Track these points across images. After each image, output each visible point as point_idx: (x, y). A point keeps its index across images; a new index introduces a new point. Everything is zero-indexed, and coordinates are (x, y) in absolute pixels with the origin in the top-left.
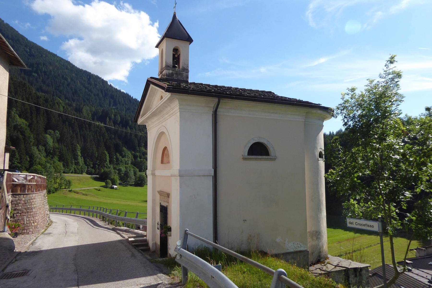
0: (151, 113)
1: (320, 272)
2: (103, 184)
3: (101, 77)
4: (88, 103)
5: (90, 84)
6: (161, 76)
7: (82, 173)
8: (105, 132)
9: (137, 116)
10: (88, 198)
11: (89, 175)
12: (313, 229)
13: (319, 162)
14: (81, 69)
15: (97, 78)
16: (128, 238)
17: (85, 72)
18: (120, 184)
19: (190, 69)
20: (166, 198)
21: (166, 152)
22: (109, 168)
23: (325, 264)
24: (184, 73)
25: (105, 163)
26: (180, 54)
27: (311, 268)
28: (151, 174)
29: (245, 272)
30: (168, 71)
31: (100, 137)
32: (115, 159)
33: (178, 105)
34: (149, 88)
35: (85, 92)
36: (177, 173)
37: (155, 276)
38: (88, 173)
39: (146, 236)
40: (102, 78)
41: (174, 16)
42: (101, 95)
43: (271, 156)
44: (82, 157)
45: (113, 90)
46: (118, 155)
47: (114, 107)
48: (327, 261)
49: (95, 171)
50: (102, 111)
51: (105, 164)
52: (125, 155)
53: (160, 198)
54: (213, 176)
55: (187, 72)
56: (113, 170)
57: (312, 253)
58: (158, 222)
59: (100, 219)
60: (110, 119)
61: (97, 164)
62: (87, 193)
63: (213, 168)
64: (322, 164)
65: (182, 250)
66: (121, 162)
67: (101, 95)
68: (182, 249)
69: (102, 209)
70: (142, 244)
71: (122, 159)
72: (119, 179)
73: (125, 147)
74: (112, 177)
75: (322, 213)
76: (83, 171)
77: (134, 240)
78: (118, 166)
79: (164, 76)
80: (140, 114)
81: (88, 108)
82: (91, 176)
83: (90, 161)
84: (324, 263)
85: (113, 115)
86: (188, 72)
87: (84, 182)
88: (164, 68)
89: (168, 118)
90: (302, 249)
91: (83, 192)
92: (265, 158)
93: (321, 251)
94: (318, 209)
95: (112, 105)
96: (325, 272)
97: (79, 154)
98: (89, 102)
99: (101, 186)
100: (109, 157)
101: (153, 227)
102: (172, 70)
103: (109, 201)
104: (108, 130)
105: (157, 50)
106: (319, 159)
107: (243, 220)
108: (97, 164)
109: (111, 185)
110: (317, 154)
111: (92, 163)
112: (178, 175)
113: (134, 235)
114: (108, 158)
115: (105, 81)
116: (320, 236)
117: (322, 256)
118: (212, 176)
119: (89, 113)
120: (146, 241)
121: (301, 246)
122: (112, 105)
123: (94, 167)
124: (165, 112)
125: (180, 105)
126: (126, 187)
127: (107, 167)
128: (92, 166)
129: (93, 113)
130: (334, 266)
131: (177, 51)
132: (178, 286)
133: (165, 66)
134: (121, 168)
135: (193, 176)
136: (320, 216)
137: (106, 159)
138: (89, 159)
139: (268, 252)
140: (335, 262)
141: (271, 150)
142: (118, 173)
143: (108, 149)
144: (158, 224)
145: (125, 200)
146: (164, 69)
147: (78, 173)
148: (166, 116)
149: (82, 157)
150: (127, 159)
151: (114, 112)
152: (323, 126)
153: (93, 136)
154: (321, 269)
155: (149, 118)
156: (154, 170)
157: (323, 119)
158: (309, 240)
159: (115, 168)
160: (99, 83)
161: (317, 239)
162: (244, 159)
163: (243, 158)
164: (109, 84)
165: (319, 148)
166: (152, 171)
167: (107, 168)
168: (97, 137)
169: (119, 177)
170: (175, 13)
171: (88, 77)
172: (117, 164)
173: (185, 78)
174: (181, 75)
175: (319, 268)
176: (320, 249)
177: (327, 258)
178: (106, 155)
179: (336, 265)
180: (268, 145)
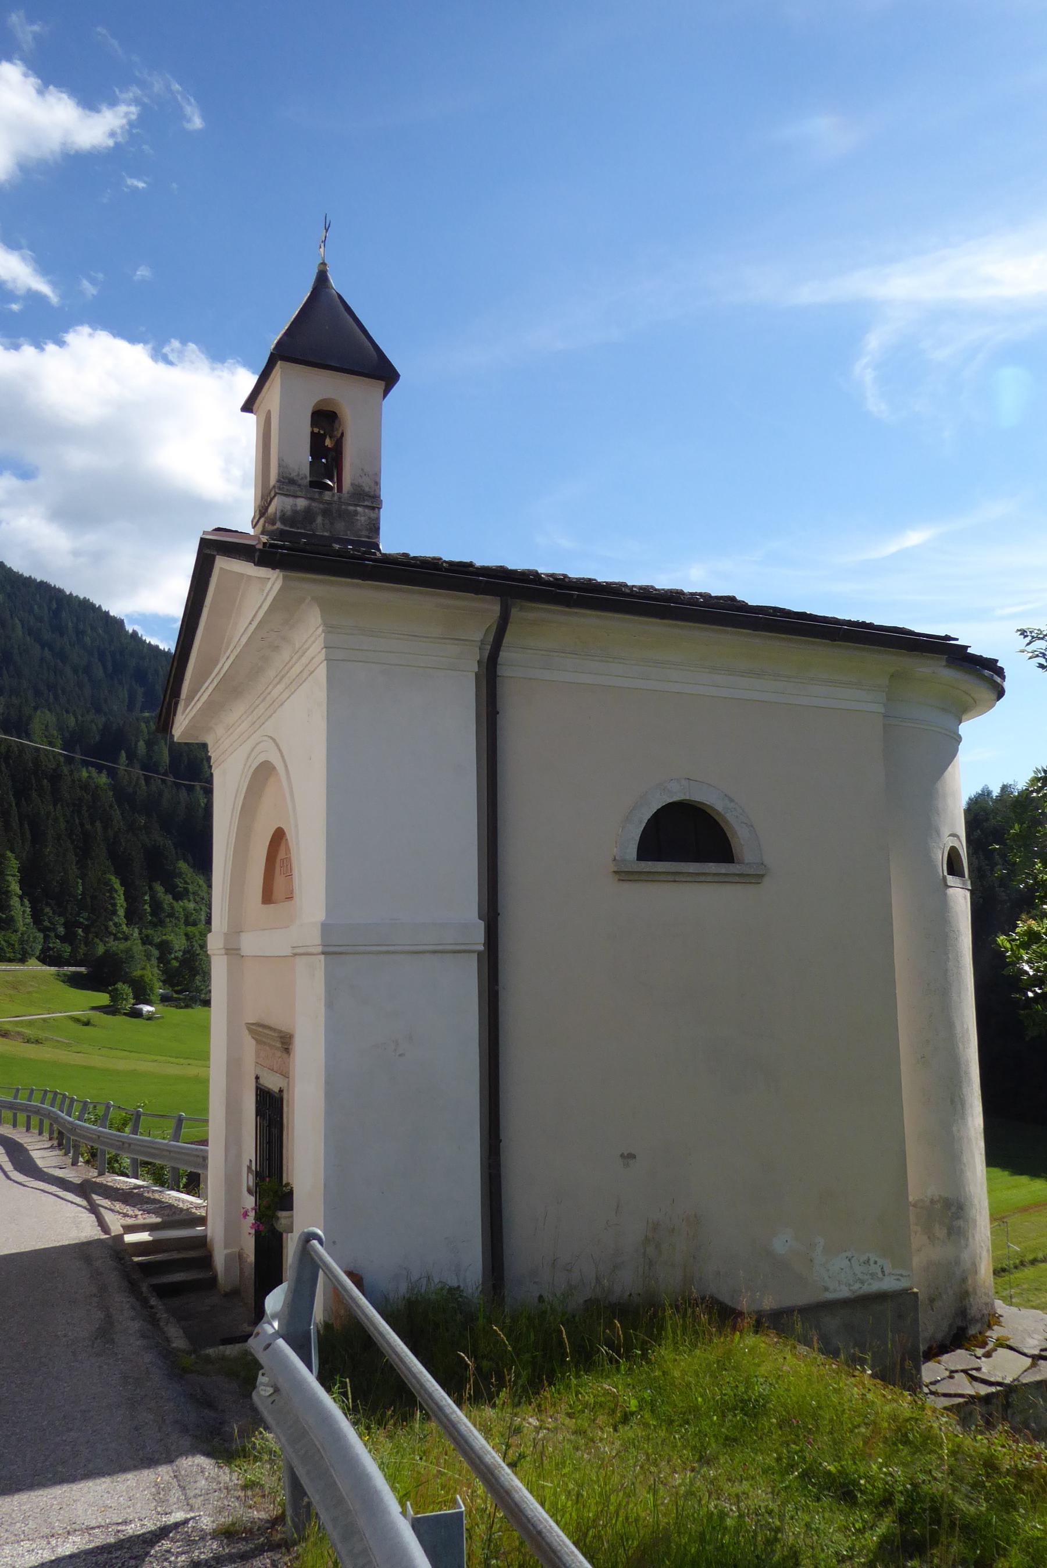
0: (215, 683)
1: (969, 1389)
2: (103, 999)
3: (100, 606)
4: (51, 699)
5: (59, 629)
6: (264, 526)
7: (23, 960)
8: (111, 806)
9: (169, 704)
10: (44, 1053)
11: (50, 966)
12: (933, 1191)
13: (950, 891)
14: (26, 578)
15: (86, 606)
16: (121, 1231)
17: (44, 586)
18: (165, 999)
19: (385, 495)
20: (278, 1054)
21: (281, 855)
22: (126, 939)
23: (988, 1348)
24: (359, 509)
25: (111, 920)
26: (342, 434)
27: (931, 1371)
28: (223, 952)
29: (632, 1414)
30: (289, 501)
31: (93, 823)
32: (147, 907)
33: (320, 629)
34: (210, 575)
35: (42, 659)
36: (313, 939)
37: (163, 1473)
38: (46, 958)
39: (202, 1221)
40: (104, 608)
41: (322, 278)
42: (99, 672)
43: (741, 862)
44: (25, 900)
45: (145, 650)
46: (159, 889)
47: (147, 714)
48: (994, 1334)
49: (74, 951)
50: (101, 727)
51: (111, 923)
52: (186, 890)
53: (258, 1056)
54: (479, 954)
55: (373, 508)
56: (138, 948)
57: (932, 1300)
58: (251, 1161)
59: (51, 1139)
60: (131, 756)
61: (80, 925)
62: (41, 1035)
63: (480, 918)
64: (961, 901)
65: (279, 1352)
66: (171, 915)
67: (99, 672)
68: (281, 1342)
69: (50, 1096)
70: (183, 1259)
71: (175, 904)
72: (164, 982)
73: (186, 860)
74: (138, 973)
75: (970, 1119)
76: (29, 950)
77: (151, 1238)
78: (159, 933)
79: (274, 524)
80: (179, 697)
81: (50, 718)
82: (56, 968)
83: (54, 913)
84: (983, 1345)
85: (141, 744)
86: (379, 508)
87: (29, 993)
88: (274, 487)
89: (285, 695)
90: (888, 1284)
91: (27, 1031)
92: (715, 874)
93: (971, 1290)
94: (952, 1102)
95: (138, 705)
96: (993, 1389)
97: (15, 888)
98: (56, 698)
99: (94, 1008)
100: (126, 900)
101: (231, 1181)
102: (306, 498)
103: (122, 1065)
104: (123, 796)
105: (251, 418)
106: (951, 880)
107: (622, 1156)
108: (81, 923)
109: (132, 1001)
110: (940, 859)
111: (62, 920)
112: (320, 949)
113: (155, 1219)
114: (120, 900)
115: (114, 618)
116: (961, 1223)
117: (973, 1312)
118: (475, 956)
119: (53, 736)
120: (202, 1243)
121: (883, 1272)
122: (138, 705)
123: (68, 938)
124: (271, 673)
125: (330, 629)
126: (190, 1010)
127: (120, 935)
128: (61, 930)
129: (67, 735)
130: (1029, 1361)
131: (334, 422)
132: (259, 1551)
133: (279, 481)
134: (170, 938)
135: (388, 952)
136: (959, 1131)
137: (114, 905)
138: (52, 908)
139: (744, 1304)
140: (1030, 1336)
141: (741, 836)
142: (158, 959)
143: (122, 867)
144: (249, 1168)
145: (182, 1061)
146: (272, 494)
147: (10, 961)
148: (280, 687)
149: (25, 900)
150: (191, 905)
151: (145, 730)
152: (960, 738)
153: (67, 822)
154: (974, 1373)
155: (213, 709)
156: (235, 931)
157: (962, 709)
158: (918, 1239)
159: (146, 941)
160: (93, 628)
161: (949, 1234)
162: (624, 875)
163: (615, 872)
164: (131, 631)
165: (945, 832)
166: (227, 936)
167: (116, 939)
168: (82, 825)
169: (164, 972)
170: (324, 264)
171: (54, 606)
172: (154, 925)
173: (365, 533)
174: (349, 517)
175: (965, 1371)
176: (964, 1280)
177: (992, 1320)
178: (112, 890)
179: (1036, 1352)
180: (730, 817)
